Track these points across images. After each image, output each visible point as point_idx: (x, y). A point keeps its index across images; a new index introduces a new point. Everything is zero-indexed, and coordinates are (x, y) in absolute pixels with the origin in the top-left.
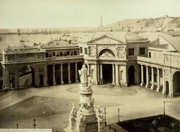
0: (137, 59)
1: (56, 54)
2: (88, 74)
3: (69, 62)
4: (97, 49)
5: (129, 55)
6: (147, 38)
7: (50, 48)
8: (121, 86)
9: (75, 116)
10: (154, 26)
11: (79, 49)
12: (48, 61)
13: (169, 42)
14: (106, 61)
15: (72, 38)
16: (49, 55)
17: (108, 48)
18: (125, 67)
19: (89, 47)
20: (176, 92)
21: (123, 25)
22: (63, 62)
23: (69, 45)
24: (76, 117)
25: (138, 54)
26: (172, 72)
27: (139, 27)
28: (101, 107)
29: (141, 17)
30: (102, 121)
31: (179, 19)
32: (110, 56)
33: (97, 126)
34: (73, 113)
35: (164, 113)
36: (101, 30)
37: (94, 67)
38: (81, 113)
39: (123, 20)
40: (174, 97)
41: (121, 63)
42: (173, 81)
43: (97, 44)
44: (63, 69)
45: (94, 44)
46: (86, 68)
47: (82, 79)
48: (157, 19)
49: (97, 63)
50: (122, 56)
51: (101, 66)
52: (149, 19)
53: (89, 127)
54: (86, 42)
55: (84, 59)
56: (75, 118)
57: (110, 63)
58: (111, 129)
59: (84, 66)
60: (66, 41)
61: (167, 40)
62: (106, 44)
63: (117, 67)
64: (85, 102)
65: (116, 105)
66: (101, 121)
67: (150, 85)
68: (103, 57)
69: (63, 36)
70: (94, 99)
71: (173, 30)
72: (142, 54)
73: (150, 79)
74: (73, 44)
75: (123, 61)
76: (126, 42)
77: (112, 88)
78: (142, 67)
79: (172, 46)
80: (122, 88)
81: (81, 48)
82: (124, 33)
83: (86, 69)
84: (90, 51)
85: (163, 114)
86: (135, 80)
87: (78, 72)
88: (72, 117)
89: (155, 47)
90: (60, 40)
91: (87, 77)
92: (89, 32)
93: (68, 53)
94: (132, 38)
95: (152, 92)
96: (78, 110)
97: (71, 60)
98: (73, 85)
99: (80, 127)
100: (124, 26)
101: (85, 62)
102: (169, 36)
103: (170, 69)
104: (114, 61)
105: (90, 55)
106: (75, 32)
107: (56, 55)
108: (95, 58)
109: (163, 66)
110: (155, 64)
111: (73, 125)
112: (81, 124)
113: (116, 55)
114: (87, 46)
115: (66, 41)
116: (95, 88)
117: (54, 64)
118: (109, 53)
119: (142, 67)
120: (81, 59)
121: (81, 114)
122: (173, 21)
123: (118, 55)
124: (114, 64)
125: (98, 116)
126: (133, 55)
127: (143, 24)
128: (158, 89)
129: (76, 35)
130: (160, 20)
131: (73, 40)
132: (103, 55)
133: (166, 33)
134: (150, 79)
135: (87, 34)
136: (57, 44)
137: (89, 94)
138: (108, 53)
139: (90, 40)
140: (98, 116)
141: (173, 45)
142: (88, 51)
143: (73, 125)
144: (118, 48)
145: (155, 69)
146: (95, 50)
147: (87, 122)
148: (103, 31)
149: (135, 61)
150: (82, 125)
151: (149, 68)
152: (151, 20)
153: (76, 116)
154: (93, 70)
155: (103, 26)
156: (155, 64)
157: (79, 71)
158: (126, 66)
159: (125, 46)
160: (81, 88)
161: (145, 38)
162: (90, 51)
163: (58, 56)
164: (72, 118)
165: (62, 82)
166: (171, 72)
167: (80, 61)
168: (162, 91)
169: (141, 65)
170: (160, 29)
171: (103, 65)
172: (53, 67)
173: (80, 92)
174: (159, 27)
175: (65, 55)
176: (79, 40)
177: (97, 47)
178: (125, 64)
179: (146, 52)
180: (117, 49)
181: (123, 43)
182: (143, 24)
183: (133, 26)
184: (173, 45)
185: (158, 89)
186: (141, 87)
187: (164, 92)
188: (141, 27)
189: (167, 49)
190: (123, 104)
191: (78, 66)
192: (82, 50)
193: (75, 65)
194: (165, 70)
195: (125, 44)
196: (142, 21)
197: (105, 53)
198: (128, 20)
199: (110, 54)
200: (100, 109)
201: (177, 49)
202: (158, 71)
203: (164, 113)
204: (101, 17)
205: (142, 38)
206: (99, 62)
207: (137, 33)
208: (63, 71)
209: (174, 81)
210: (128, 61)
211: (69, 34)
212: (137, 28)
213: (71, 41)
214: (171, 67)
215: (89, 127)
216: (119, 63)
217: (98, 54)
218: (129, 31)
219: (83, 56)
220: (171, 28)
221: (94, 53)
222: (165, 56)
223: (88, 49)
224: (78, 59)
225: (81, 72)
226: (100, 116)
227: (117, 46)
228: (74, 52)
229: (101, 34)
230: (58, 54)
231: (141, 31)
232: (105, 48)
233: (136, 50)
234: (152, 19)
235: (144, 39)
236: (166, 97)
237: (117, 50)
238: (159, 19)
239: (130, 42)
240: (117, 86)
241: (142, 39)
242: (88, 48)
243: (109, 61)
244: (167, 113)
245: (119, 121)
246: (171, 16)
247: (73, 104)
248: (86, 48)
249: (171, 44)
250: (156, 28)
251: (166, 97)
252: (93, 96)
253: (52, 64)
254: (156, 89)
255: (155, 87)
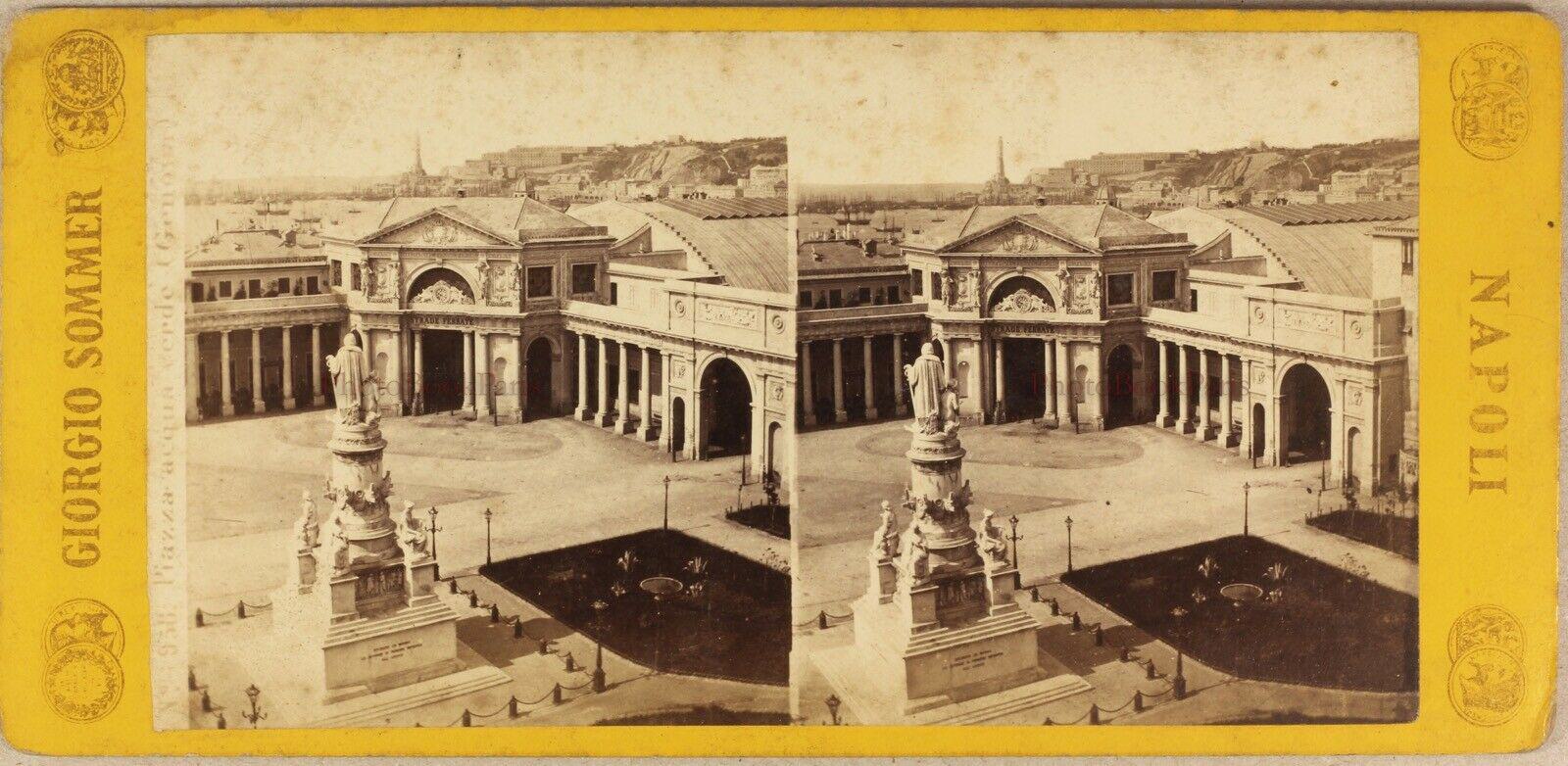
0: (563, 312)
1: (234, 289)
2: (946, 379)
3: (317, 321)
4: (401, 270)
5: (1111, 303)
6: (1182, 232)
7: (211, 263)
8: (499, 419)
9: (312, 542)
10: (1212, 183)
11: (326, 267)
12: (203, 319)
13: (690, 244)
14: (435, 318)
15: (878, 230)
16: (206, 290)
17: (447, 266)
18: (515, 343)
19: (370, 262)
20: (1290, 449)
21: (1088, 177)
22: (263, 320)
23: (284, 252)
24: (898, 555)
25: (1149, 299)
26: (1278, 369)
27: (569, 178)
28: (417, 505)
29: (579, 141)
30: (1003, 568)
31: (725, 150)
32: (1034, 304)
33: (400, 579)
34: (885, 540)
35: (1246, 527)
36: (415, 191)
37: (970, 354)
38: (337, 529)
39: (1088, 158)
40: (1282, 464)
41: (499, 329)
42: (701, 398)
43: (401, 250)
44: (263, 352)
45: (388, 249)
46: (935, 354)
47: (919, 399)
48: (644, 150)
49: (401, 328)
50: (507, 296)
51: (417, 337)
52: (610, 149)
53: (371, 585)
54: (355, 239)
55: (928, 321)
56: (314, 550)
57: (452, 327)
58: (458, 590)
59: (927, 348)
60: (275, 232)
61: (682, 235)
62: (437, 250)
63: (480, 343)
64: (353, 489)
65: (1060, 503)
66: (418, 562)
67: (1192, 420)
68: (428, 303)
69: (260, 213)
70: (967, 482)
71: (704, 195)
72: (1162, 298)
73: (612, 393)
74: (305, 247)
75: (506, 320)
76: (521, 239)
77: (1042, 439)
78: (582, 343)
79: (700, 259)
80: (1083, 436)
81: (337, 263)
82: (512, 205)
83: (937, 359)
84: (372, 276)
85: (1243, 532)
86: (553, 397)
87: (903, 370)
88: (302, 545)
89: (633, 263)
90: (832, 239)
91: (941, 392)
92: (370, 197)
93: (863, 297)
94: (541, 223)
95: (1203, 448)
96: (327, 516)
97: (876, 322)
98: (302, 418)
99: (332, 585)
100: (1094, 183)
101: (353, 323)
102: (1276, 228)
103: (1269, 355)
104: (469, 319)
105: (372, 293)
106: (891, 206)
107: (813, 304)
108: (974, 316)
109: (1243, 344)
110: (1214, 337)
111: (888, 587)
112: (919, 582)
113: (1058, 300)
114: (359, 257)
115: (275, 232)
116: (394, 430)
117: (838, 335)
118: (1032, 292)
119: (582, 343)
120: (915, 319)
121: (337, 534)
122: (703, 160)
123: (1067, 303)
124: (1050, 338)
125: (987, 552)
126: (549, 292)
127: (587, 167)
128: (642, 431)
129: (315, 208)
130: (652, 154)
131: (885, 241)
132: (426, 294)
133: (675, 205)
134: (612, 393)
135: (359, 204)
136: (819, 259)
137: (369, 453)
138: (1026, 295)
139: (372, 229)
140: (987, 552)
141: (1283, 261)
142: (364, 279)
143: (888, 587)
144: (488, 267)
145: (633, 350)
146: (395, 272)
147: (943, 576)
148: (1011, 202)
149: (1137, 328)
150: (923, 585)
151: (1192, 352)
152: (1199, 158)
153: (898, 551)
154: (965, 366)
155: (1007, 181)
156: (1214, 337)
157: (330, 357)
158: (519, 338)
159: (515, 259)
160: (917, 438)
161: (1175, 230)
162: (372, 276)
163: (240, 295)
164: (880, 562)
165: (259, 403)
166: (695, 361)
167: (333, 317)
168: (658, 438)
169: (578, 336)
170: (651, 190)
171: (426, 334)
172: (251, 340)
173: (913, 454)
174: (1231, 189)
175: (853, 304)
176: (328, 230)
177: (401, 260)
178: (1095, 338)
179: (1177, 288)
180: (481, 270)
181: (505, 243)
182: (587, 167)
183: (545, 175)
184: (1283, 261)
185: (642, 431)
186: (1158, 430)
187: (1247, 449)
188: (1161, 187)
189: (1259, 278)
190: (1085, 502)
191: (904, 349)
192: (338, 273)
193: (310, 334)
194: (1250, 362)
195: (514, 251)
196: (584, 154)
197: (434, 287)
198: (1110, 157)
199: (1033, 297)
200: (415, 515)
201: (718, 270)
202: (645, 356)
203: (1246, 527)
204: (1001, 142)
205: (582, 226)
206: (407, 322)
207: (563, 204)
208: (262, 360)
209: (1284, 402)
210: (1108, 325)
211: (868, 216)
212: (1144, 192)
213: (878, 246)
214: (695, 344)
215: (952, 595)
216: (489, 329)
217: (408, 285)
218: (1111, 204)
219: (925, 307)
220: (697, 184)
221: (968, 293)
222: (674, 298)
223: (363, 271)
224: (906, 319)
225: (917, 372)
226: (994, 550)
227: (482, 258)
228: (305, 282)
229: (423, 205)
230: (243, 287)
231: (1159, 204)
232: (435, 266)
233: (1139, 279)
234: (621, 149)
235: (1171, 235)
236: (675, 461)
237: (483, 275)
238: (650, 148)
239: (1115, 248)
240: (1065, 428)
241: (585, 229)
242: (366, 265)
243: (448, 318)
244: (1257, 530)
245: (489, 559)
246: (697, 139)
247: (306, 494)
248: (355, 266)
249: (694, 249)
250: (640, 184)
251: (1255, 467)
252: (388, 462)
253: (219, 329)
254: (635, 431)
255: (631, 425)
